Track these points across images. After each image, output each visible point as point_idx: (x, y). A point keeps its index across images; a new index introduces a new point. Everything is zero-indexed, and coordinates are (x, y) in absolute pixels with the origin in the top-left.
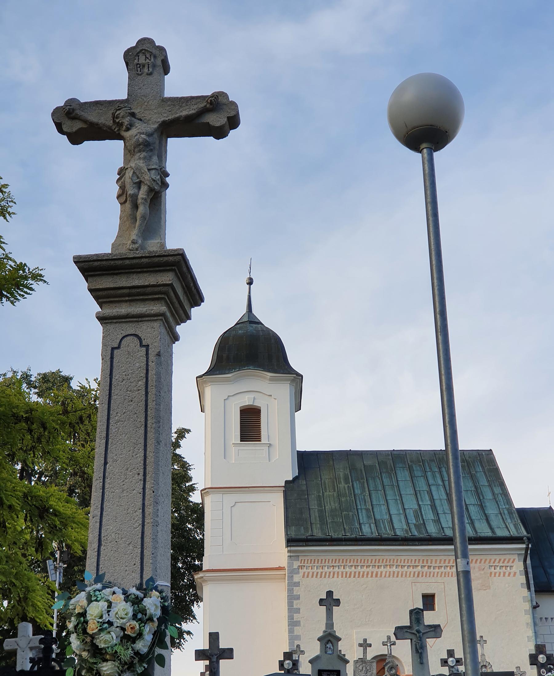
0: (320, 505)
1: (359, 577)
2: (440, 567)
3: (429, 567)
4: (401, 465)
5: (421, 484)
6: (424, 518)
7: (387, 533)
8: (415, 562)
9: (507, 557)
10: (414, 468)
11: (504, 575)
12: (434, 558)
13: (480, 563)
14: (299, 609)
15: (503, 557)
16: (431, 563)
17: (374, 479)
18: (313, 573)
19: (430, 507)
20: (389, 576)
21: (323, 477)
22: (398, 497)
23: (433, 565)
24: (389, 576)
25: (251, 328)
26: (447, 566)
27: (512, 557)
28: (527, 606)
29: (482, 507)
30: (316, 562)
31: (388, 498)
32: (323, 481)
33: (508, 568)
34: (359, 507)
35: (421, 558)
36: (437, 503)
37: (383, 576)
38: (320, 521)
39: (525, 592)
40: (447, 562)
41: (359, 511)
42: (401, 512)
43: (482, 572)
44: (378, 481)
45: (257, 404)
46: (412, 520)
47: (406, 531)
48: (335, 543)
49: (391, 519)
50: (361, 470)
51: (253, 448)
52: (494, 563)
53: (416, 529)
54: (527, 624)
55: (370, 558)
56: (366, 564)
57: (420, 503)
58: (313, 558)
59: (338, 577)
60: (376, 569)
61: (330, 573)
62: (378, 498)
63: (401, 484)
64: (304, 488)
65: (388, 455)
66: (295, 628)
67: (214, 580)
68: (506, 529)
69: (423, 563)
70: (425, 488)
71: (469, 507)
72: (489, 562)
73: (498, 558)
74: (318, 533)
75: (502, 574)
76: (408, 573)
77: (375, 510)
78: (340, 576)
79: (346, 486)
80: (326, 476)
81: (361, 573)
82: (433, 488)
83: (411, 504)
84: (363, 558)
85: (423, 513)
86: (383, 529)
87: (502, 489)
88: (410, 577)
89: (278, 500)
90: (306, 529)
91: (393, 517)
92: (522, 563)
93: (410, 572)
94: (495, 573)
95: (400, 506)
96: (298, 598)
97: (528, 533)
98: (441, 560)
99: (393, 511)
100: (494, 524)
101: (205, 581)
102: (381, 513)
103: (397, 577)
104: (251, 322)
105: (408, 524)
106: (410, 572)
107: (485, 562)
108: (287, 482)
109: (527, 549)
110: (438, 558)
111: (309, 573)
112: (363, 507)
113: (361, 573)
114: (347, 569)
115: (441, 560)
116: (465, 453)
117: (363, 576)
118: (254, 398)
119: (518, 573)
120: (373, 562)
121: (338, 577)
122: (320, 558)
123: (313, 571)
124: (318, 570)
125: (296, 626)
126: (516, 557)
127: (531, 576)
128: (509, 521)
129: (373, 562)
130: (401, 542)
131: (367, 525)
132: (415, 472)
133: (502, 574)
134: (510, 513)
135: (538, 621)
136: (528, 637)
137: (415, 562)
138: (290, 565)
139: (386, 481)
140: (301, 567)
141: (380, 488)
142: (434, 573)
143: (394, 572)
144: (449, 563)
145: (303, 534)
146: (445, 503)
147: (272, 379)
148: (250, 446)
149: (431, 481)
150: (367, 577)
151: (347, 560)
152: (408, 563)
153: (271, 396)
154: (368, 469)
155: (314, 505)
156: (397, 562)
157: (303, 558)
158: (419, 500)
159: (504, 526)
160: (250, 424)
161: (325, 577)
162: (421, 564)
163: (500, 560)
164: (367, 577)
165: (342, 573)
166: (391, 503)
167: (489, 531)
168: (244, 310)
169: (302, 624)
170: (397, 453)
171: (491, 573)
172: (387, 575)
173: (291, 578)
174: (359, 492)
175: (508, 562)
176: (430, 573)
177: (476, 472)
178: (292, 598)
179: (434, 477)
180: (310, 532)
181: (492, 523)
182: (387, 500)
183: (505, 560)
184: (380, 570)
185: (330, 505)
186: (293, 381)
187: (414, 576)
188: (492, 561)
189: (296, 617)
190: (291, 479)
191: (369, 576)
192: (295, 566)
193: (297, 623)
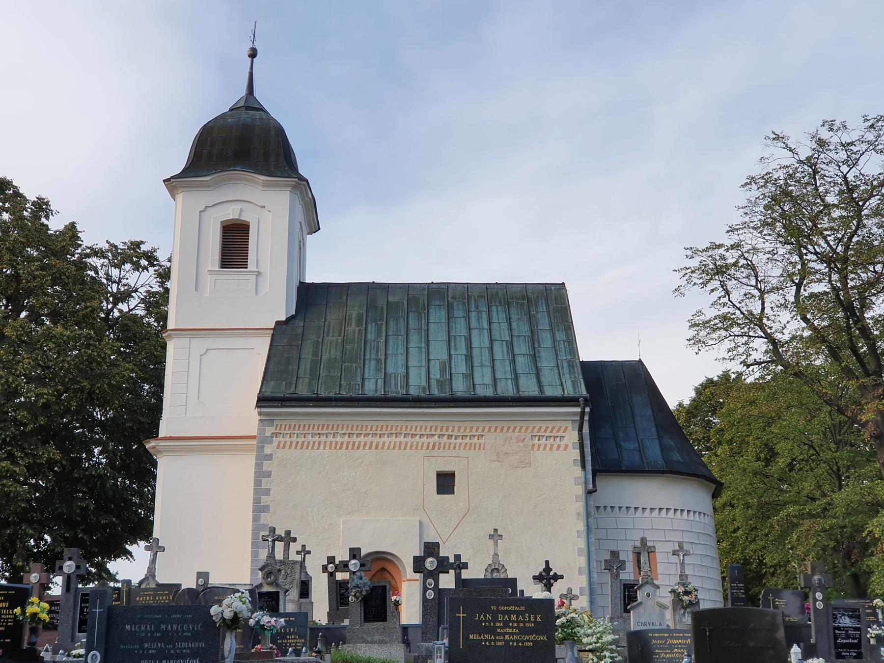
0: (315, 354)
1: (353, 448)
2: (464, 437)
3: (450, 437)
4: (437, 303)
6: (453, 372)
7: (397, 390)
8: (431, 430)
9: (557, 424)
10: (455, 307)
11: (551, 449)
12: (457, 425)
13: (519, 431)
14: (269, 490)
15: (551, 425)
16: (453, 431)
18: (292, 442)
19: (464, 357)
20: (394, 448)
21: (328, 317)
22: (423, 345)
23: (456, 433)
24: (394, 448)
25: (245, 116)
26: (474, 436)
27: (564, 424)
28: (580, 490)
29: (534, 358)
30: (297, 428)
31: (411, 345)
32: (327, 323)
33: (558, 439)
34: (368, 357)
35: (439, 425)
36: (476, 352)
37: (386, 447)
38: (310, 374)
39: (578, 472)
40: (474, 429)
41: (367, 362)
42: (424, 364)
43: (522, 445)
44: (402, 324)
45: (245, 218)
46: (436, 374)
47: (424, 388)
48: (322, 403)
49: (407, 373)
50: (382, 308)
51: (236, 277)
52: (538, 431)
53: (438, 386)
54: (579, 514)
55: (370, 424)
56: (364, 432)
57: (452, 352)
58: (293, 423)
59: (324, 448)
60: (377, 439)
61: (314, 442)
62: (396, 346)
63: (432, 327)
64: (300, 331)
65: (424, 289)
66: (262, 514)
67: (169, 450)
68: (559, 388)
69: (442, 430)
70: (464, 332)
71: (516, 357)
72: (532, 431)
73: (544, 425)
74: (303, 391)
75: (548, 447)
76: (420, 444)
77: (388, 361)
78: (328, 448)
79: (357, 329)
80: (333, 317)
81: (357, 443)
82: (475, 333)
83: (439, 352)
84: (360, 424)
85: (453, 366)
86: (393, 386)
87: (567, 336)
88: (422, 448)
89: (263, 345)
90: (289, 385)
91: (411, 371)
92: (576, 433)
93: (423, 443)
94: (539, 446)
95: (424, 355)
96: (269, 475)
97: (588, 392)
98: (466, 428)
99: (413, 362)
100: (545, 380)
101: (160, 452)
102: (395, 366)
103: (405, 449)
104: (248, 108)
105: (429, 378)
106: (423, 443)
107: (526, 431)
109: (583, 414)
110: (463, 425)
111: (285, 442)
112: (373, 356)
113: (357, 443)
115: (466, 428)
116: (528, 287)
117: (358, 447)
118: (241, 211)
119: (571, 445)
120: (374, 429)
121: (324, 448)
122: (302, 423)
123: (291, 439)
124: (299, 439)
125: (264, 512)
126: (569, 424)
127: (588, 450)
128: (567, 376)
129: (374, 429)
130: (412, 404)
131: (373, 381)
132: (455, 312)
133: (548, 447)
134: (571, 366)
135: (592, 510)
136: (578, 531)
137: (431, 430)
138: (261, 431)
139: (413, 323)
140: (276, 435)
142: (455, 444)
143: (401, 443)
144: (477, 431)
145: (284, 391)
146: (486, 352)
147: (266, 185)
148: (232, 274)
149: (474, 324)
150: (364, 448)
151: (338, 426)
152: (421, 430)
153: (264, 207)
154: (392, 307)
155: (307, 354)
156: (406, 429)
157: (279, 423)
158: (452, 348)
159: (558, 383)
160: (235, 243)
161: (307, 448)
162: (438, 432)
163: (547, 428)
164: (364, 448)
165: (331, 442)
166: (413, 352)
167: (537, 388)
168: (243, 92)
169: (271, 509)
170: (436, 286)
171: (533, 445)
172: (392, 446)
173: (261, 448)
174: (373, 337)
175: (558, 431)
176: (450, 444)
177: (537, 312)
178: (261, 474)
179: (479, 319)
180: (293, 389)
181: (543, 379)
182: (407, 348)
183: (553, 428)
184: (382, 439)
185: (330, 353)
186: (295, 187)
187: (427, 448)
188: (536, 429)
189: (264, 500)
190: (284, 319)
191: (367, 447)
192: (268, 434)
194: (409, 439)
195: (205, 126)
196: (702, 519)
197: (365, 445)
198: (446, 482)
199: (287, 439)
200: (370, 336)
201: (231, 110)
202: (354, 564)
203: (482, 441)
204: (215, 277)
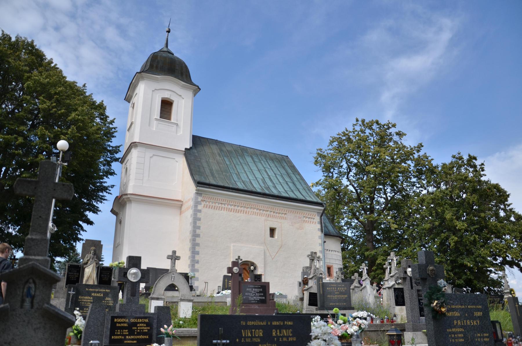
3: (274, 212)
5: (260, 165)
9: (312, 213)
17: (234, 158)
23: (276, 211)
28: (320, 241)
39: (319, 233)
45: (173, 98)
46: (263, 185)
62: (239, 168)
70: (263, 168)
73: (308, 213)
99: (251, 178)
102: (244, 177)
108: (186, 149)
114: (211, 204)
116: (202, 140)
126: (316, 214)
141: (239, 164)
169: (201, 236)
185: (215, 167)
189: (198, 231)
193: (198, 236)
194: (258, 211)
195: (186, 67)
196: (336, 253)
197: (241, 211)
198: (272, 231)
199: (211, 204)
200: (228, 163)
201: (160, 51)
202: (134, 274)
203: (286, 216)
204: (158, 122)
